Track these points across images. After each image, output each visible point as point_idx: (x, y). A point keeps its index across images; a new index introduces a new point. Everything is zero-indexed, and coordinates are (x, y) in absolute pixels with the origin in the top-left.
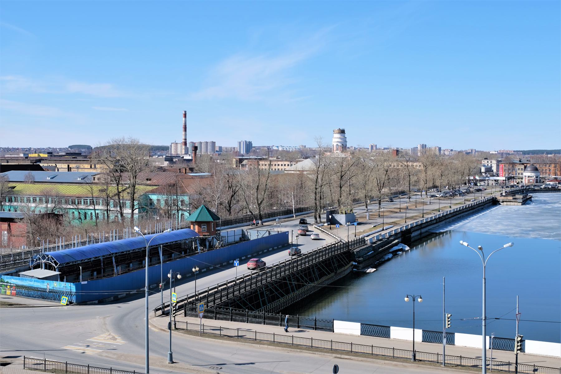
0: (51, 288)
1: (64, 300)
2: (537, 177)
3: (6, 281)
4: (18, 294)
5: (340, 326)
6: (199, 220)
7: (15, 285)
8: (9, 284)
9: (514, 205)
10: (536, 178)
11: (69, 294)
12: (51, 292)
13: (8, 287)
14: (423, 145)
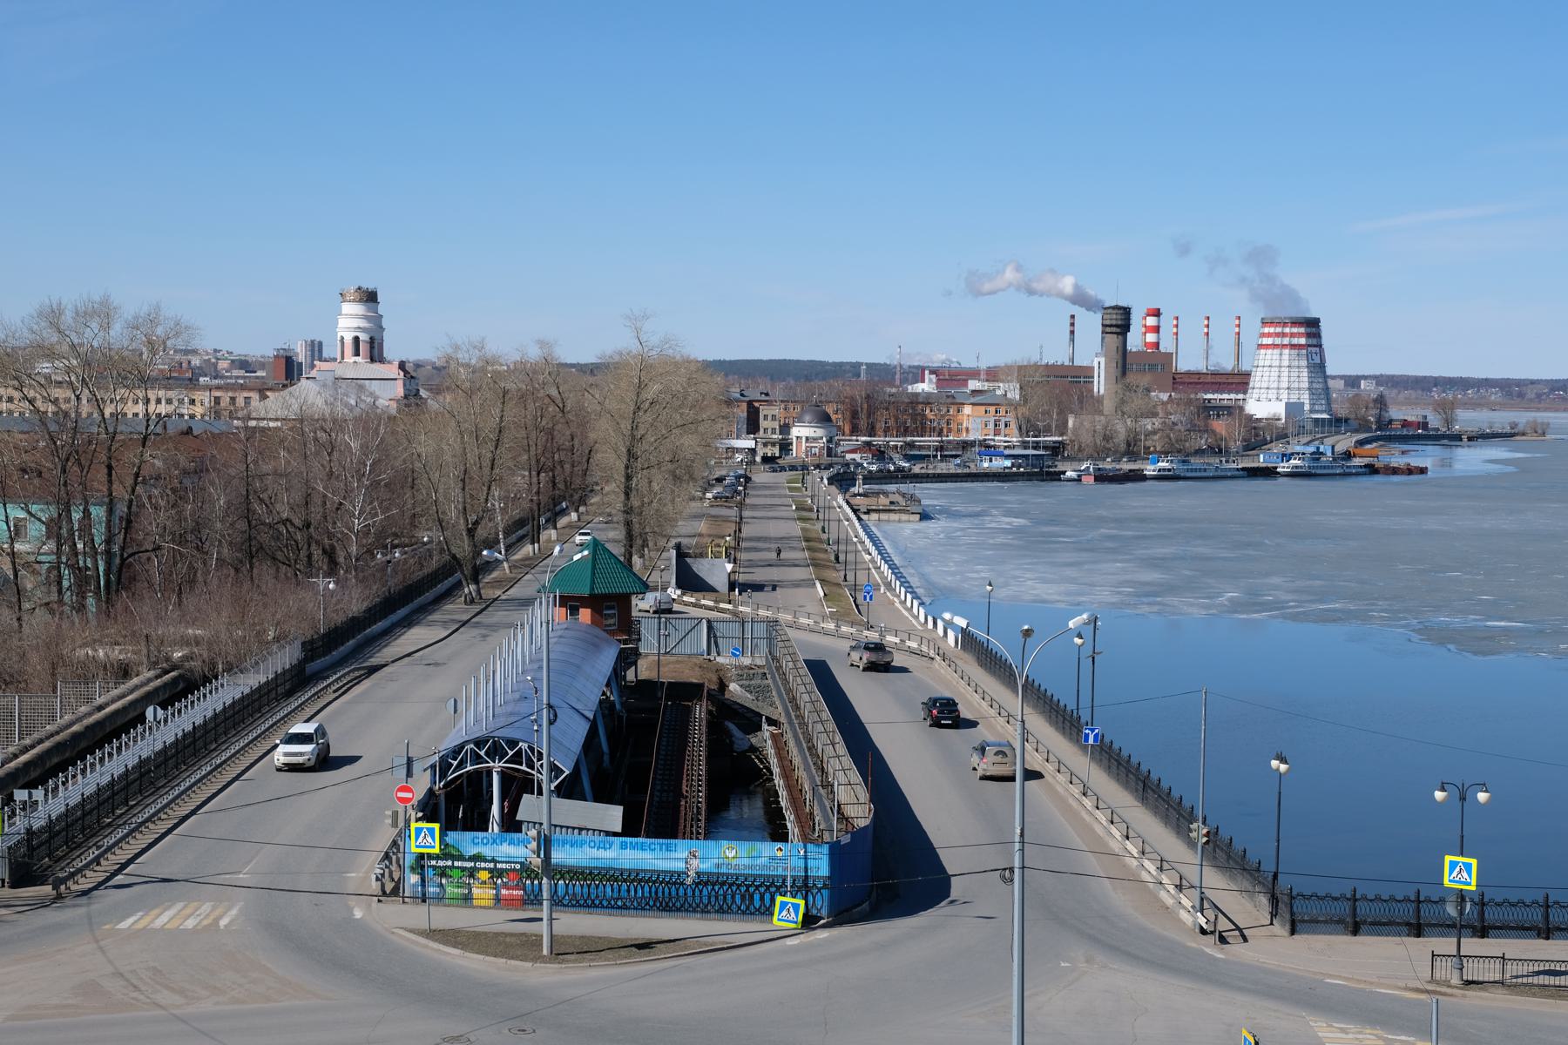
0: (706, 866)
1: (788, 911)
2: (830, 441)
3: (472, 851)
6: (601, 589)
7: (518, 867)
8: (483, 865)
9: (899, 521)
10: (828, 442)
11: (804, 887)
12: (706, 884)
13: (484, 875)
14: (313, 342)
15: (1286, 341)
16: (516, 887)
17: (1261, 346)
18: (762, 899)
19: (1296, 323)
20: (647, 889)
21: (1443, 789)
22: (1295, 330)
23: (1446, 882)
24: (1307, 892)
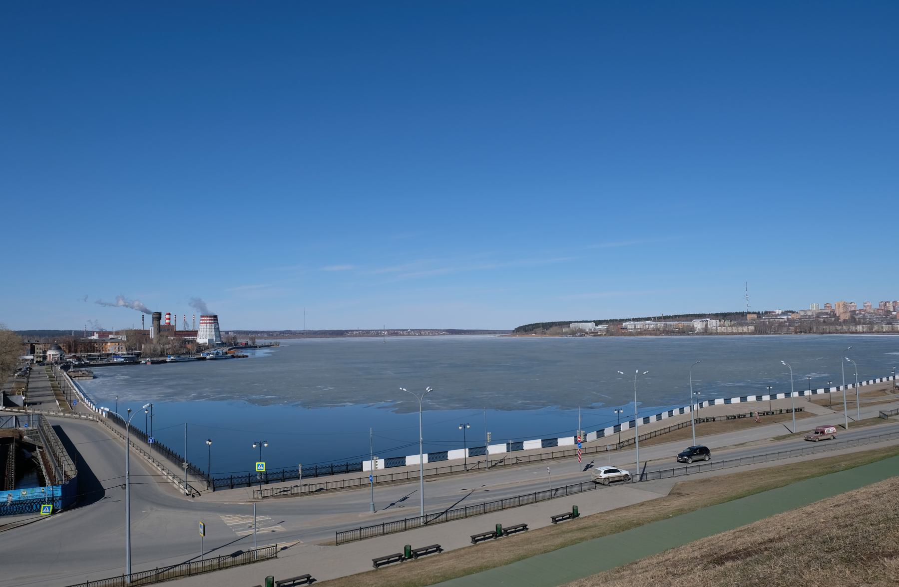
2: (61, 355)
5: (367, 465)
9: (86, 379)
11: (52, 500)
12: (15, 505)
15: (208, 322)
17: (201, 323)
22: (210, 318)
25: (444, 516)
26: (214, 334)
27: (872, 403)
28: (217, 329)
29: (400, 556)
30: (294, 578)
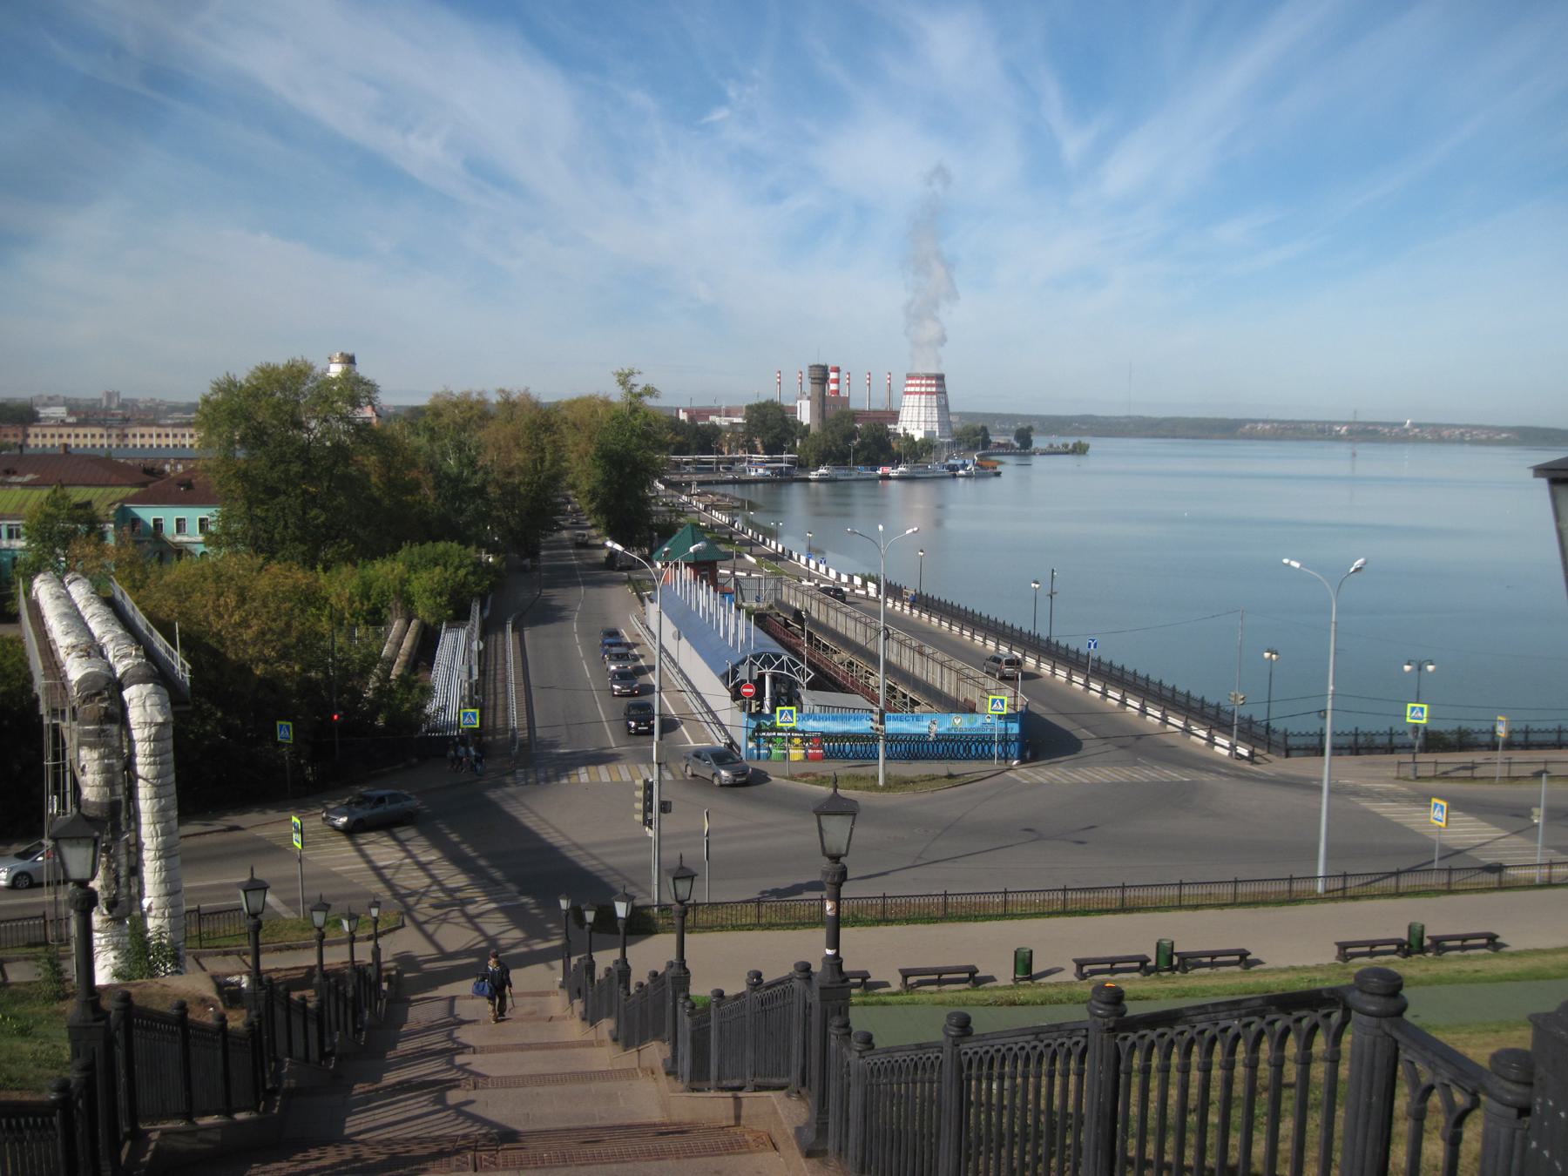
4: (829, 756)
12: (940, 741)
13: (797, 741)
15: (923, 389)
16: (819, 748)
17: (907, 393)
18: (977, 749)
19: (929, 377)
20: (903, 746)
21: (1409, 664)
22: (929, 382)
23: (279, 739)
24: (1536, 729)
25: (1391, 882)
26: (936, 419)
27: (56, 744)
28: (944, 408)
29: (1143, 961)
30: (1466, 935)
